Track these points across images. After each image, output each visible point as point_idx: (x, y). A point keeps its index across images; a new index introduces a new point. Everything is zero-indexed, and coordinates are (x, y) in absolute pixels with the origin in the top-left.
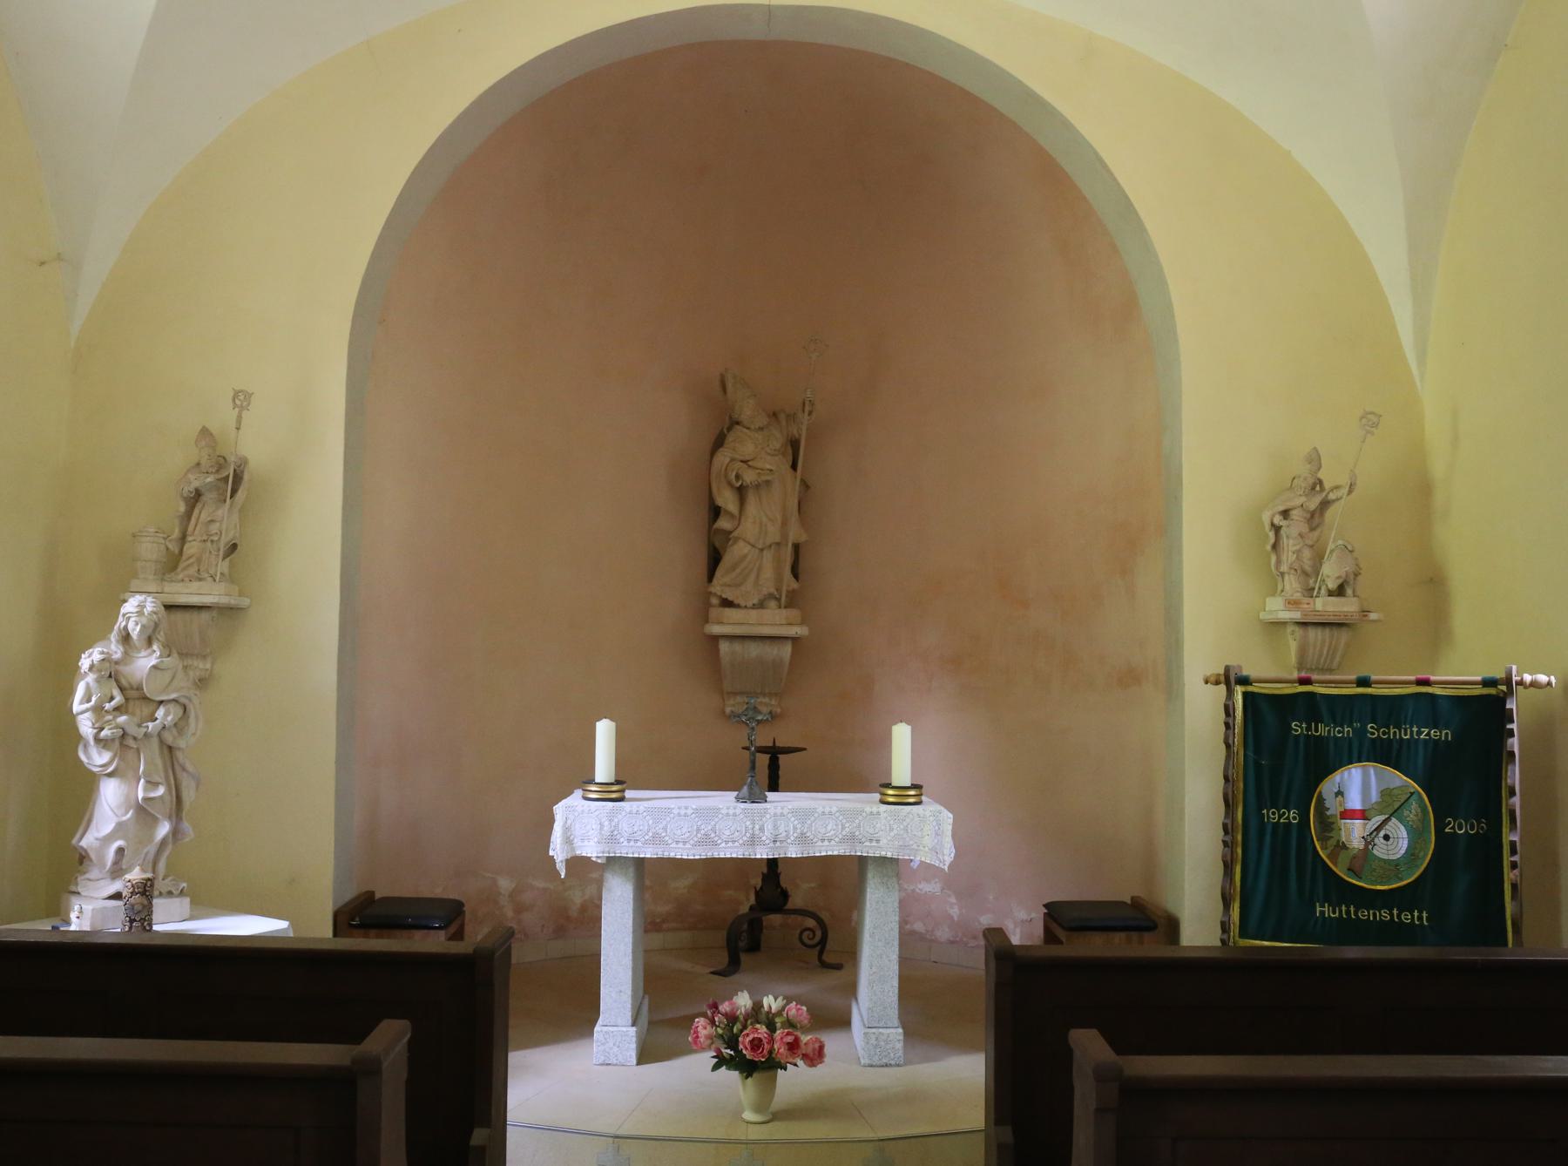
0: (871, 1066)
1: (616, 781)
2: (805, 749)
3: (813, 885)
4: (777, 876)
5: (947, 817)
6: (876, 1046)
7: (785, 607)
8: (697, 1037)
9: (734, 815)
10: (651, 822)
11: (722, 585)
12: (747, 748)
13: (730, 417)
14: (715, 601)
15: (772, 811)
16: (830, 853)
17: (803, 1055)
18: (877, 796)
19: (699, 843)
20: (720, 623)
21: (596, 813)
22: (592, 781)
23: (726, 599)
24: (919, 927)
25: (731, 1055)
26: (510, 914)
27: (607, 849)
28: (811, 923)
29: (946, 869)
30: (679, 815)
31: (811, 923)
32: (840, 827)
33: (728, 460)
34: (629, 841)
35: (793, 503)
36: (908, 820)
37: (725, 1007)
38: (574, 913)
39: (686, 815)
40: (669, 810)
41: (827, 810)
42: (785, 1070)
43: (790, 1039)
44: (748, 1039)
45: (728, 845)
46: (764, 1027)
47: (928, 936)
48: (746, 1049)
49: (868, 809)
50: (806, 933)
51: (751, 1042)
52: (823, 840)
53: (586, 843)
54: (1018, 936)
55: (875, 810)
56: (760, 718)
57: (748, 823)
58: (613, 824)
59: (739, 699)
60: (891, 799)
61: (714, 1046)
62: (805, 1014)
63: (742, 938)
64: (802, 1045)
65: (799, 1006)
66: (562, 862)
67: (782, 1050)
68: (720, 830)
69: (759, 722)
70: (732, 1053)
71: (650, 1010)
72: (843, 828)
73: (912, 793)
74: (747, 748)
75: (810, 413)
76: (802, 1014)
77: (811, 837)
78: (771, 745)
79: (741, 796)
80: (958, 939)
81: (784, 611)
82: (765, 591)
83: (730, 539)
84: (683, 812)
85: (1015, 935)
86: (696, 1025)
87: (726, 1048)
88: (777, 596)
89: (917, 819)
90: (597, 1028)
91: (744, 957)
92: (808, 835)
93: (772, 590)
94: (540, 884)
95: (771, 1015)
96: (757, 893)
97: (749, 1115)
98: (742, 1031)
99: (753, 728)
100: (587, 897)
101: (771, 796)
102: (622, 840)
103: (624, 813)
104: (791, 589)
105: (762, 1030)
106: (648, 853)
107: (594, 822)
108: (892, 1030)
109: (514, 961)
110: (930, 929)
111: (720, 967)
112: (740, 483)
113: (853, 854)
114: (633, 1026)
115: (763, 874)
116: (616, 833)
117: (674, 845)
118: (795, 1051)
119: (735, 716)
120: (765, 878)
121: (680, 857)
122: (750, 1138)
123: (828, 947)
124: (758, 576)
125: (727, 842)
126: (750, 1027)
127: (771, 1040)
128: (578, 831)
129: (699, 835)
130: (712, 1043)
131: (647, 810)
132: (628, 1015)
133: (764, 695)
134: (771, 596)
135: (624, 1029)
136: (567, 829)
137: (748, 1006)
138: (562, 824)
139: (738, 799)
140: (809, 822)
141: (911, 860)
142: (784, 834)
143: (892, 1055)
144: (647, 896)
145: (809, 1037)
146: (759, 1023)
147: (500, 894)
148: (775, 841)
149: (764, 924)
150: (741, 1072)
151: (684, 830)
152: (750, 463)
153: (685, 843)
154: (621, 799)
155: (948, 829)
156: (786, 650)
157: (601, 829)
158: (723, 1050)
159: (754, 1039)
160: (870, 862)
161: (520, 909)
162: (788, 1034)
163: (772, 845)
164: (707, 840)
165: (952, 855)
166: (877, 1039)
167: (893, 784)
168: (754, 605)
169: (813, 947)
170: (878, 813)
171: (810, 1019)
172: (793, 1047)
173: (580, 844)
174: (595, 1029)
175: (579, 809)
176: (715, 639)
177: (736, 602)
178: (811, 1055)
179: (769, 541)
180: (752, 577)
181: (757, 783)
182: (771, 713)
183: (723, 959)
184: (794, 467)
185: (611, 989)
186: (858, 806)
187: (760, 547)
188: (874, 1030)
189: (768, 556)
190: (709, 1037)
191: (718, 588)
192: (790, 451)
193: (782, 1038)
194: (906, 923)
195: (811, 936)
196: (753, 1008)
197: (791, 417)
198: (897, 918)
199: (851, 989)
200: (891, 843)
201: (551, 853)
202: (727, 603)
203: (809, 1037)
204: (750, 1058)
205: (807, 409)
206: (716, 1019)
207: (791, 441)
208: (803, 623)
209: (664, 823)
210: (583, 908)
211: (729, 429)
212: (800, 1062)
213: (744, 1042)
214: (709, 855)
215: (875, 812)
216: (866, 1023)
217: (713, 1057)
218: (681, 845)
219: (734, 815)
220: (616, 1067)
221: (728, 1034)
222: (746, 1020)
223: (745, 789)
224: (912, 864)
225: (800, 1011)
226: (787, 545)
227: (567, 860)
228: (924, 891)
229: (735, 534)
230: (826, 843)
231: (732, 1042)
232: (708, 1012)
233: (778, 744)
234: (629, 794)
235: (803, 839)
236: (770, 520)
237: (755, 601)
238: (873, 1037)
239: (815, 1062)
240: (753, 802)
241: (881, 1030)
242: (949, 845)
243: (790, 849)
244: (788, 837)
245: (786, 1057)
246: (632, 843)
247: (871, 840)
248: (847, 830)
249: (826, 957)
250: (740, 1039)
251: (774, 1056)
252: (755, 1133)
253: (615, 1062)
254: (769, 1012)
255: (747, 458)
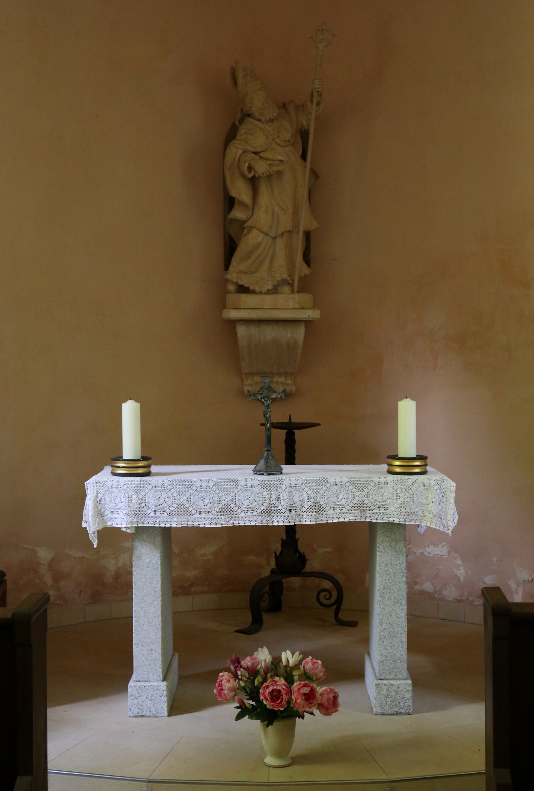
0: (383, 714)
1: (142, 457)
2: (319, 425)
3: (329, 550)
4: (296, 541)
5: (451, 486)
6: (387, 696)
7: (298, 292)
8: (222, 690)
9: (253, 486)
10: (175, 494)
11: (238, 272)
12: (263, 425)
13: (242, 110)
14: (231, 287)
15: (287, 482)
16: (341, 520)
17: (319, 704)
18: (385, 467)
19: (220, 513)
20: (237, 308)
21: (125, 487)
22: (120, 458)
23: (242, 286)
24: (428, 587)
25: (252, 705)
26: (49, 580)
27: (135, 520)
28: (327, 584)
29: (450, 532)
30: (201, 487)
31: (327, 584)
32: (350, 496)
33: (240, 152)
34: (155, 512)
35: (303, 192)
36: (414, 489)
37: (247, 662)
38: (109, 579)
39: (207, 487)
40: (192, 483)
41: (338, 480)
42: (303, 718)
43: (306, 690)
44: (268, 691)
45: (298, 513)
46: (282, 679)
47: (436, 596)
48: (266, 699)
49: (376, 479)
50: (323, 594)
51: (271, 693)
52: (335, 508)
53: (116, 515)
54: (520, 595)
55: (383, 479)
56: (274, 396)
57: (265, 494)
58: (140, 497)
59: (257, 379)
60: (398, 470)
61: (236, 698)
62: (320, 668)
63: (264, 599)
64: (318, 695)
65: (315, 660)
66: (94, 532)
67: (299, 701)
68: (240, 500)
69: (274, 400)
70: (254, 703)
71: (181, 666)
72: (354, 497)
73: (417, 463)
74: (263, 425)
75: (318, 104)
76: (318, 667)
77: (324, 505)
78: (287, 420)
79: (258, 468)
80: (464, 598)
81: (297, 296)
82: (278, 278)
83: (244, 228)
84: (205, 484)
85: (517, 594)
86: (220, 679)
87: (248, 699)
88: (290, 282)
89: (422, 487)
90: (131, 684)
91: (266, 617)
92: (321, 503)
93: (285, 276)
94: (76, 553)
95: (288, 669)
96: (277, 558)
97: (270, 760)
98: (262, 683)
99: (268, 406)
100: (120, 565)
101: (286, 468)
102: (149, 511)
103: (150, 487)
104: (302, 275)
105: (281, 682)
106: (174, 523)
107: (122, 495)
108: (402, 682)
109: (49, 625)
110: (438, 588)
111: (246, 626)
112: (252, 174)
113: (363, 520)
114: (164, 680)
115: (282, 540)
116: (143, 505)
117: (197, 515)
118: (311, 701)
119: (251, 396)
120: (284, 544)
121: (203, 526)
122: (271, 780)
123: (343, 607)
124: (271, 262)
125: (246, 512)
126: (269, 680)
127: (289, 691)
128: (108, 504)
129: (220, 506)
130: (236, 695)
131: (171, 483)
132: (159, 672)
133: (280, 375)
134: (284, 282)
135: (156, 684)
136: (98, 503)
137: (267, 661)
138: (92, 498)
139: (255, 472)
140: (322, 492)
141: (418, 526)
142: (299, 503)
143: (402, 704)
144: (176, 562)
145: (324, 688)
146: (278, 676)
147: (40, 564)
148: (290, 510)
149: (284, 585)
150: (263, 721)
151: (207, 501)
152: (261, 155)
153: (207, 513)
154: (148, 474)
155: (451, 496)
156: (300, 333)
157: (130, 502)
158: (246, 702)
159: (273, 691)
160: (379, 528)
161: (58, 577)
162: (305, 685)
163: (287, 513)
164: (227, 510)
165: (456, 521)
166: (388, 690)
167: (400, 455)
168: (268, 290)
169: (331, 606)
170: (386, 483)
171: (326, 671)
172: (310, 697)
173: (110, 516)
174: (129, 685)
175: (109, 484)
176: (233, 323)
177: (252, 288)
178: (326, 704)
179: (281, 229)
180: (267, 263)
181: (273, 457)
182: (284, 391)
183: (248, 618)
184: (304, 157)
185: (143, 648)
186: (367, 476)
187: (273, 235)
188: (385, 682)
189: (281, 243)
190: (233, 689)
191: (235, 275)
192: (299, 140)
193: (299, 689)
194: (416, 584)
195: (327, 597)
196: (272, 662)
197: (301, 108)
198: (405, 579)
199: (366, 641)
200: (398, 510)
201: (84, 525)
202: (243, 290)
203: (324, 688)
204: (271, 708)
205: (315, 100)
206: (239, 673)
207: (300, 132)
208: (315, 306)
209: (188, 495)
210: (117, 575)
211: (241, 121)
212: (316, 712)
213: (264, 694)
214: (230, 524)
215: (383, 482)
216: (378, 675)
217: (237, 707)
218: (203, 515)
219: (253, 486)
220: (150, 719)
221: (250, 687)
222: (266, 674)
223: (262, 462)
224: (419, 529)
225: (316, 665)
226: (298, 232)
227: (99, 531)
228: (432, 553)
229: (249, 224)
230: (338, 511)
231: (254, 694)
232: (232, 667)
233: (293, 421)
234: (154, 469)
235: (316, 507)
236: (283, 209)
237: (270, 287)
238: (385, 688)
239: (330, 711)
240: (270, 474)
241: (391, 682)
242: (452, 512)
243: (305, 517)
244: (302, 506)
245: (303, 706)
246: (158, 514)
247: (379, 508)
248: (357, 498)
249: (342, 616)
250: (261, 691)
251: (292, 705)
252: (276, 776)
253: (148, 714)
254: (287, 666)
255: (259, 150)
